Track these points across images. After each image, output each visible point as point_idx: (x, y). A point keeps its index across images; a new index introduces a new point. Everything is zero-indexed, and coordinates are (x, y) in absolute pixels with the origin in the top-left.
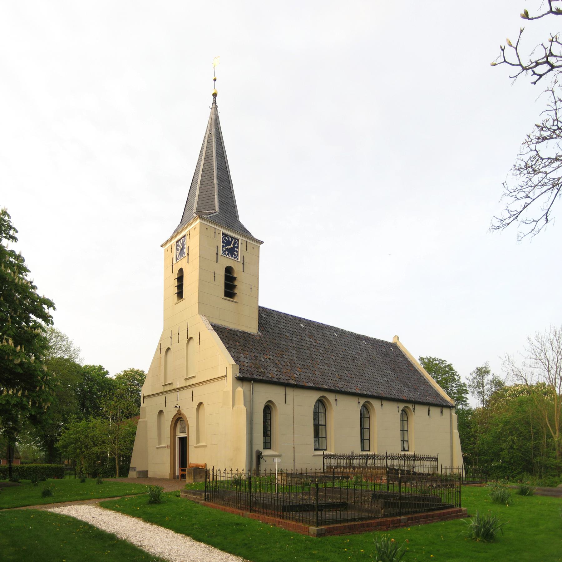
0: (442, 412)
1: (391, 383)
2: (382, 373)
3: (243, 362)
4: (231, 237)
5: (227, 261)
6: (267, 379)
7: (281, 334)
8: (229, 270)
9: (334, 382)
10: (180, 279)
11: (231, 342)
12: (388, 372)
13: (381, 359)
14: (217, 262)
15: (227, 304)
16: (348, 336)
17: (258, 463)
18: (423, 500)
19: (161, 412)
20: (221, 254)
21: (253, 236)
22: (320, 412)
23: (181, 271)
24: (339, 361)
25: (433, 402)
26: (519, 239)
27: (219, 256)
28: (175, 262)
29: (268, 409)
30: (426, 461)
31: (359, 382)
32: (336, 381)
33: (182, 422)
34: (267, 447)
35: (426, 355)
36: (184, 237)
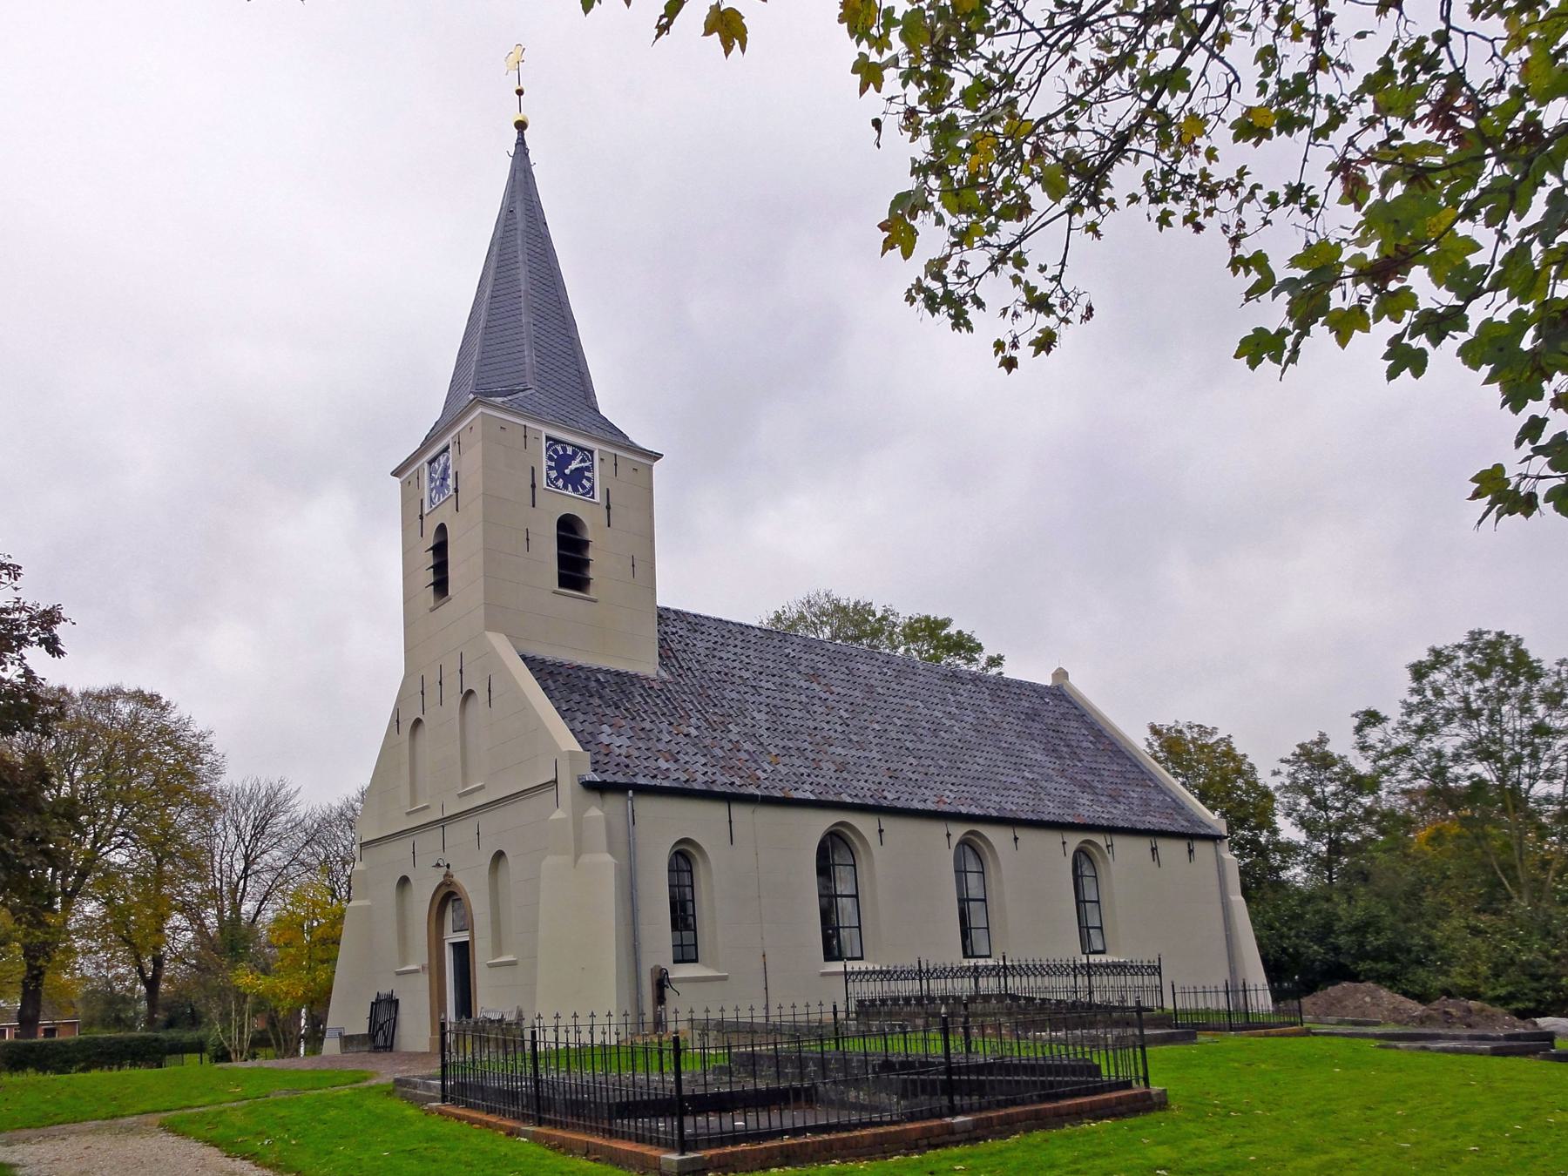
0: (1191, 851)
1: (1044, 784)
2: (1018, 760)
3: (608, 745)
5: (568, 502)
6: (675, 785)
7: (726, 674)
8: (569, 528)
9: (874, 787)
10: (440, 549)
11: (576, 697)
12: (1034, 756)
13: (1016, 728)
14: (534, 506)
15: (570, 601)
16: (924, 673)
17: (660, 999)
19: (404, 881)
20: (545, 486)
21: (632, 443)
22: (836, 862)
23: (442, 529)
24: (893, 735)
25: (1164, 827)
28: (426, 511)
29: (683, 858)
30: (1148, 974)
31: (949, 785)
32: (880, 783)
33: (456, 904)
34: (685, 958)
35: (1178, 714)
36: (446, 449)
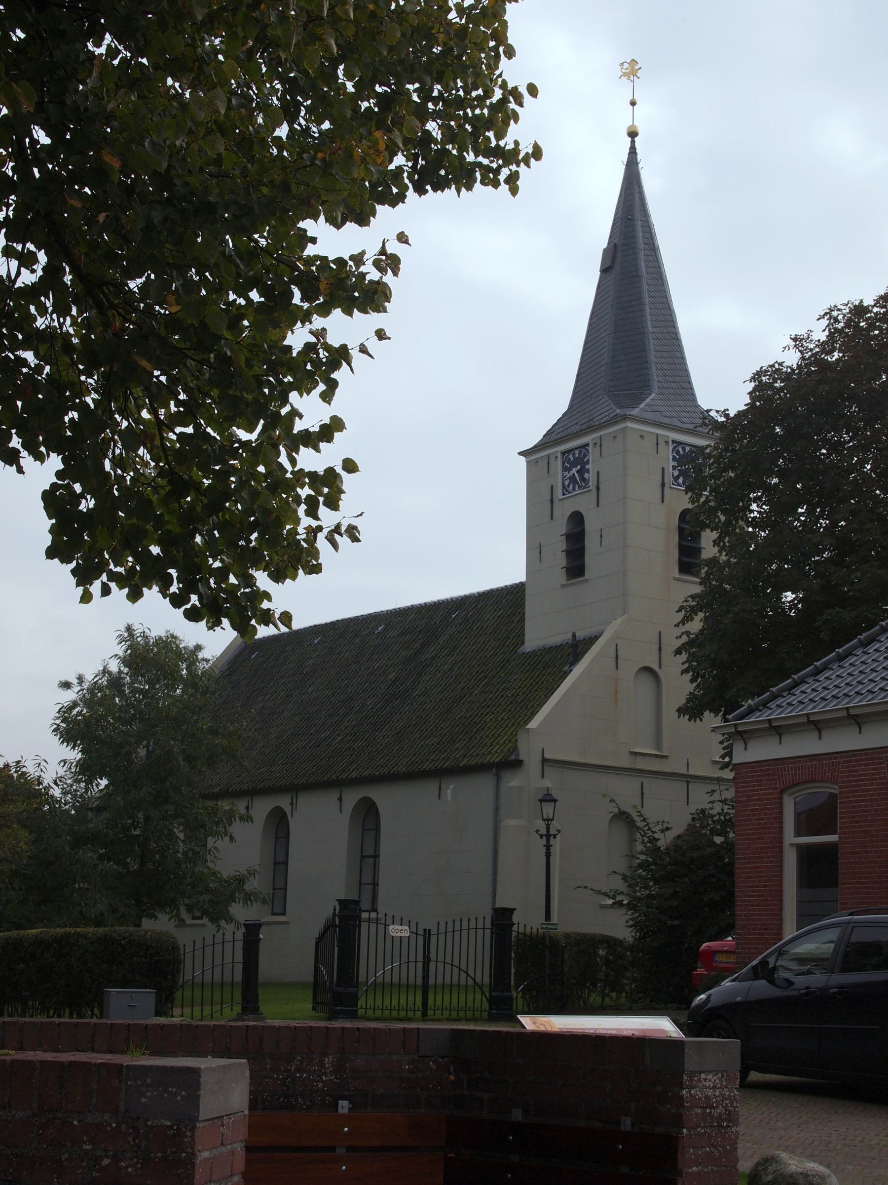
4: (688, 445)
18: (160, 115)
26: (538, 831)
27: (666, 489)
